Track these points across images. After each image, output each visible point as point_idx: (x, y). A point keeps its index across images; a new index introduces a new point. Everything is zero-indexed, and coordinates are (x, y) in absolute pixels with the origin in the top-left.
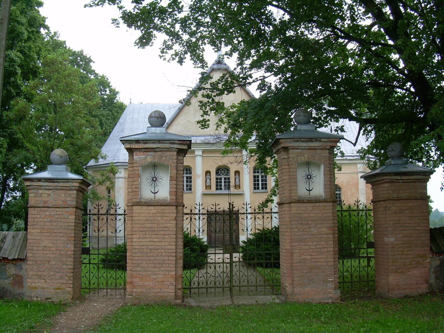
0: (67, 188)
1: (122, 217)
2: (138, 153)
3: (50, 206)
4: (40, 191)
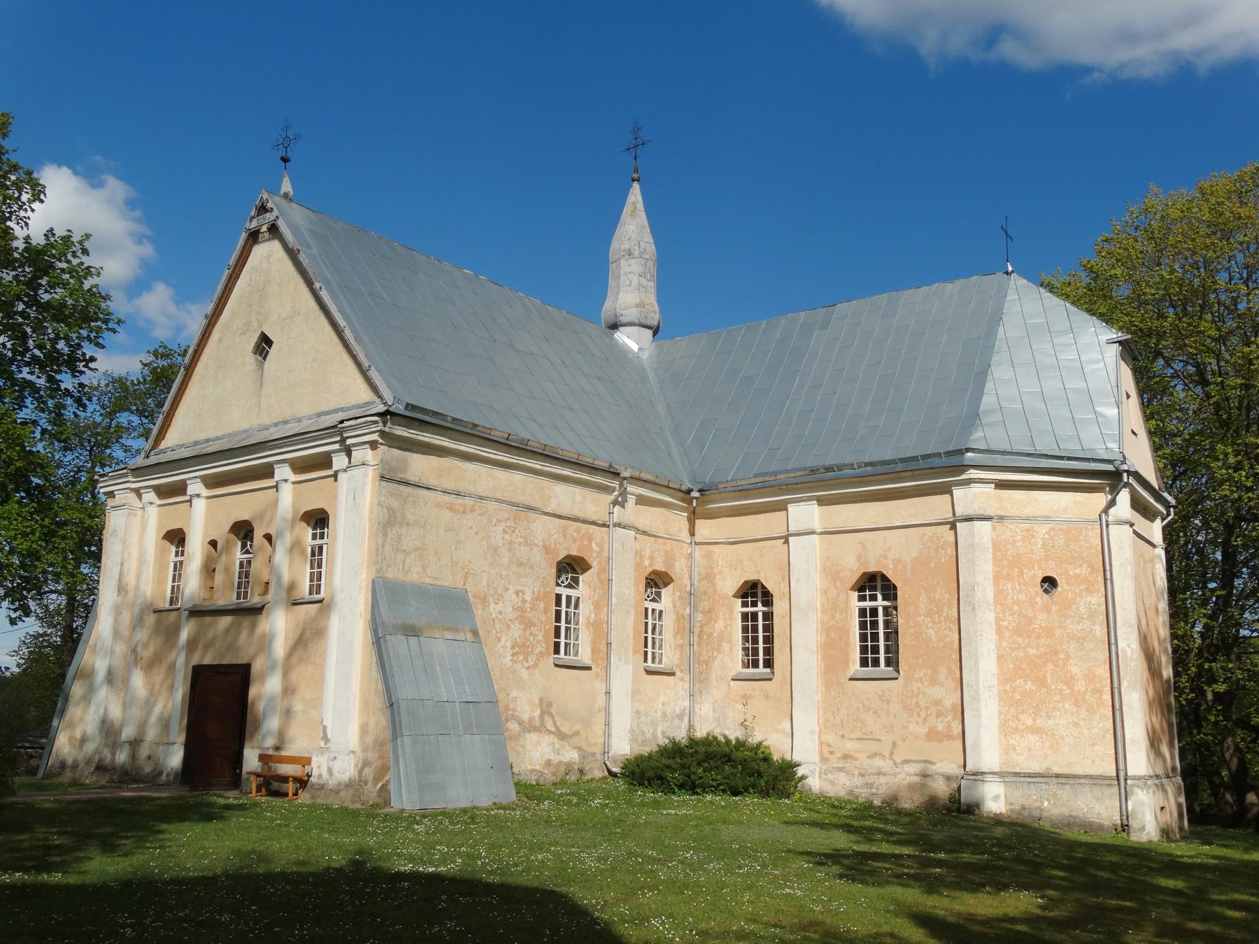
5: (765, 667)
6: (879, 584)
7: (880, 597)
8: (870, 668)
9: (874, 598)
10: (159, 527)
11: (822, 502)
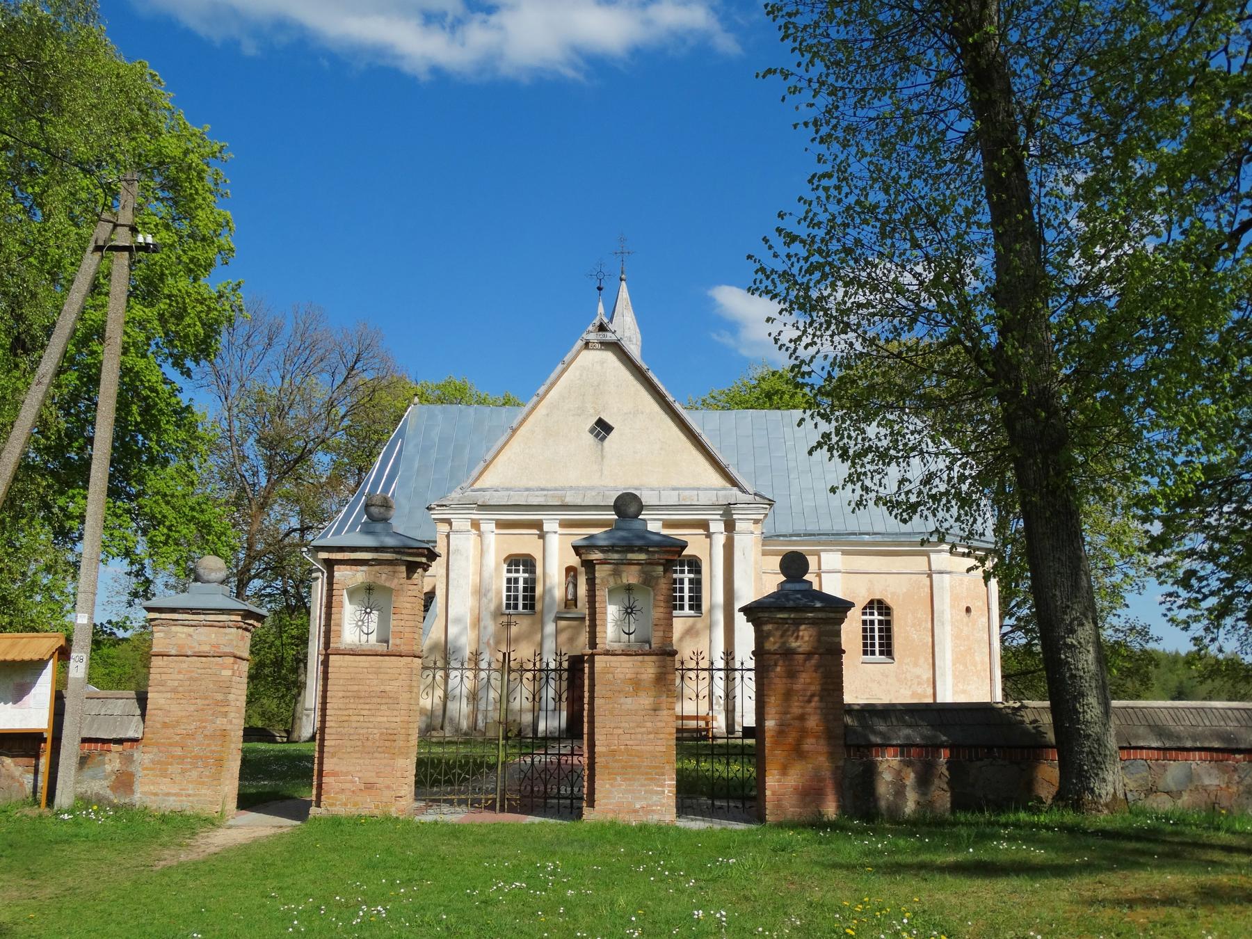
0: (221, 624)
1: (722, 674)
2: (342, 567)
3: (189, 653)
4: (174, 628)
5: (881, 653)
6: (876, 606)
7: (876, 613)
8: (869, 657)
9: (872, 614)
10: (498, 551)
11: (844, 553)
